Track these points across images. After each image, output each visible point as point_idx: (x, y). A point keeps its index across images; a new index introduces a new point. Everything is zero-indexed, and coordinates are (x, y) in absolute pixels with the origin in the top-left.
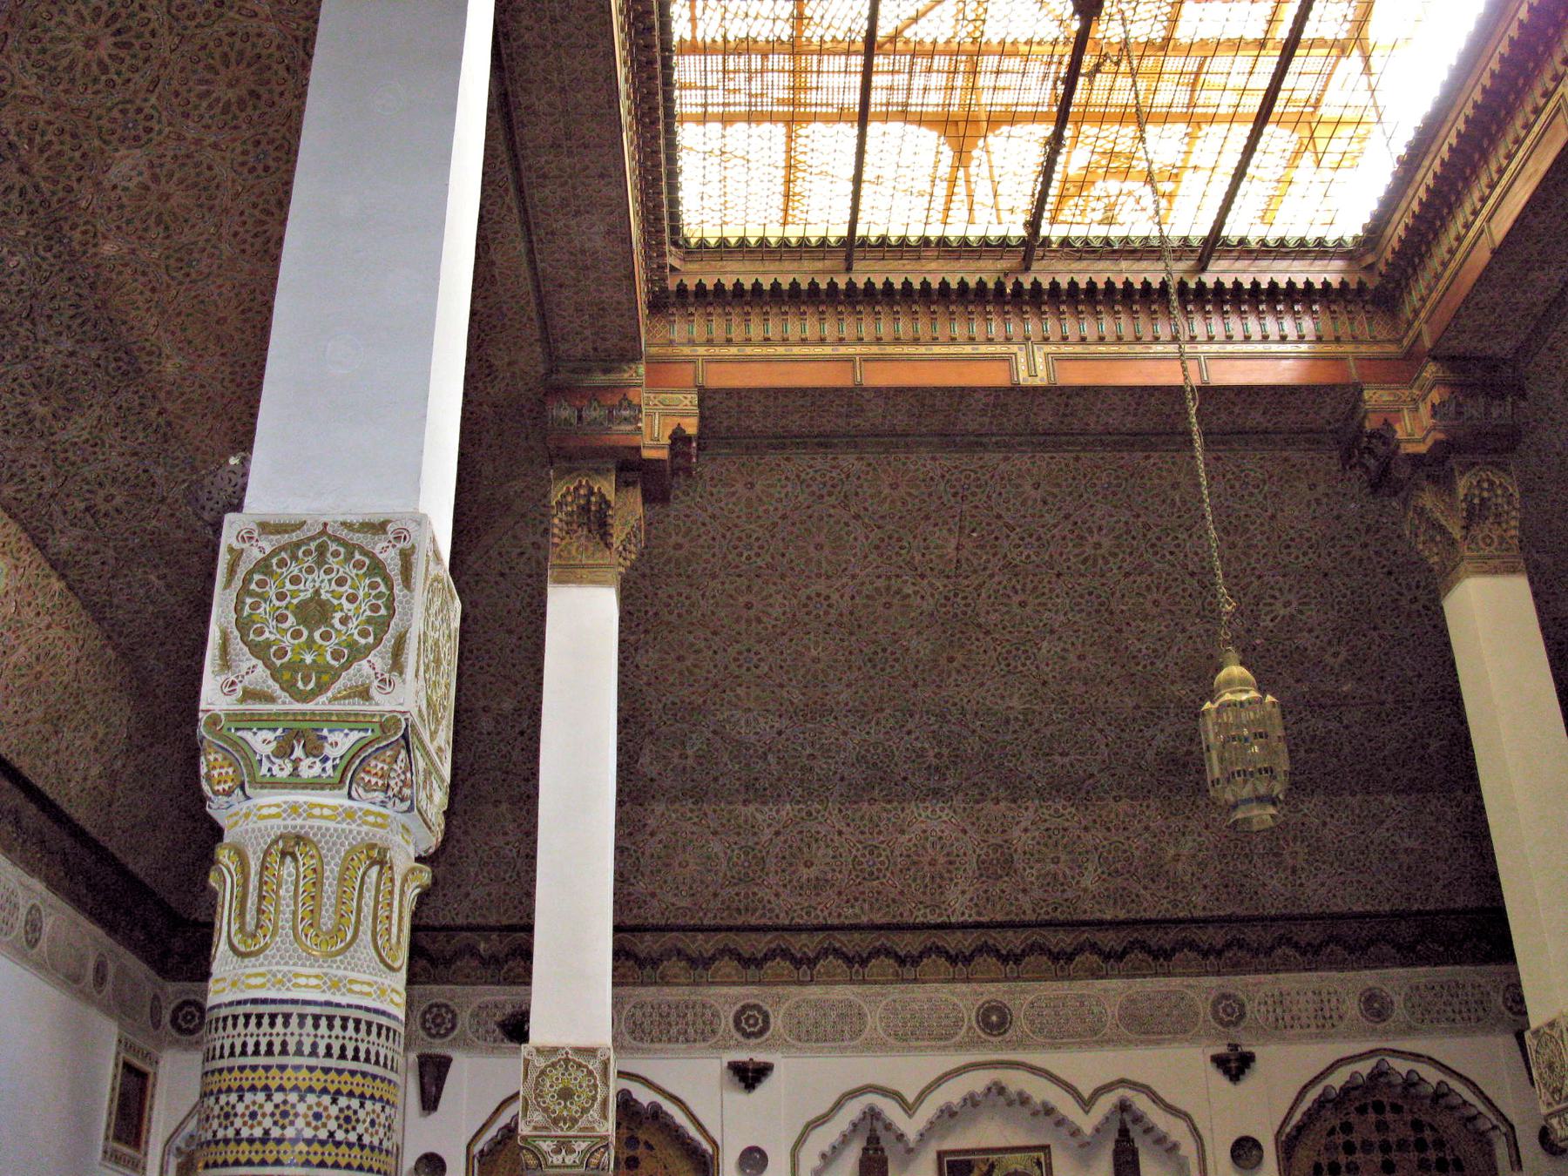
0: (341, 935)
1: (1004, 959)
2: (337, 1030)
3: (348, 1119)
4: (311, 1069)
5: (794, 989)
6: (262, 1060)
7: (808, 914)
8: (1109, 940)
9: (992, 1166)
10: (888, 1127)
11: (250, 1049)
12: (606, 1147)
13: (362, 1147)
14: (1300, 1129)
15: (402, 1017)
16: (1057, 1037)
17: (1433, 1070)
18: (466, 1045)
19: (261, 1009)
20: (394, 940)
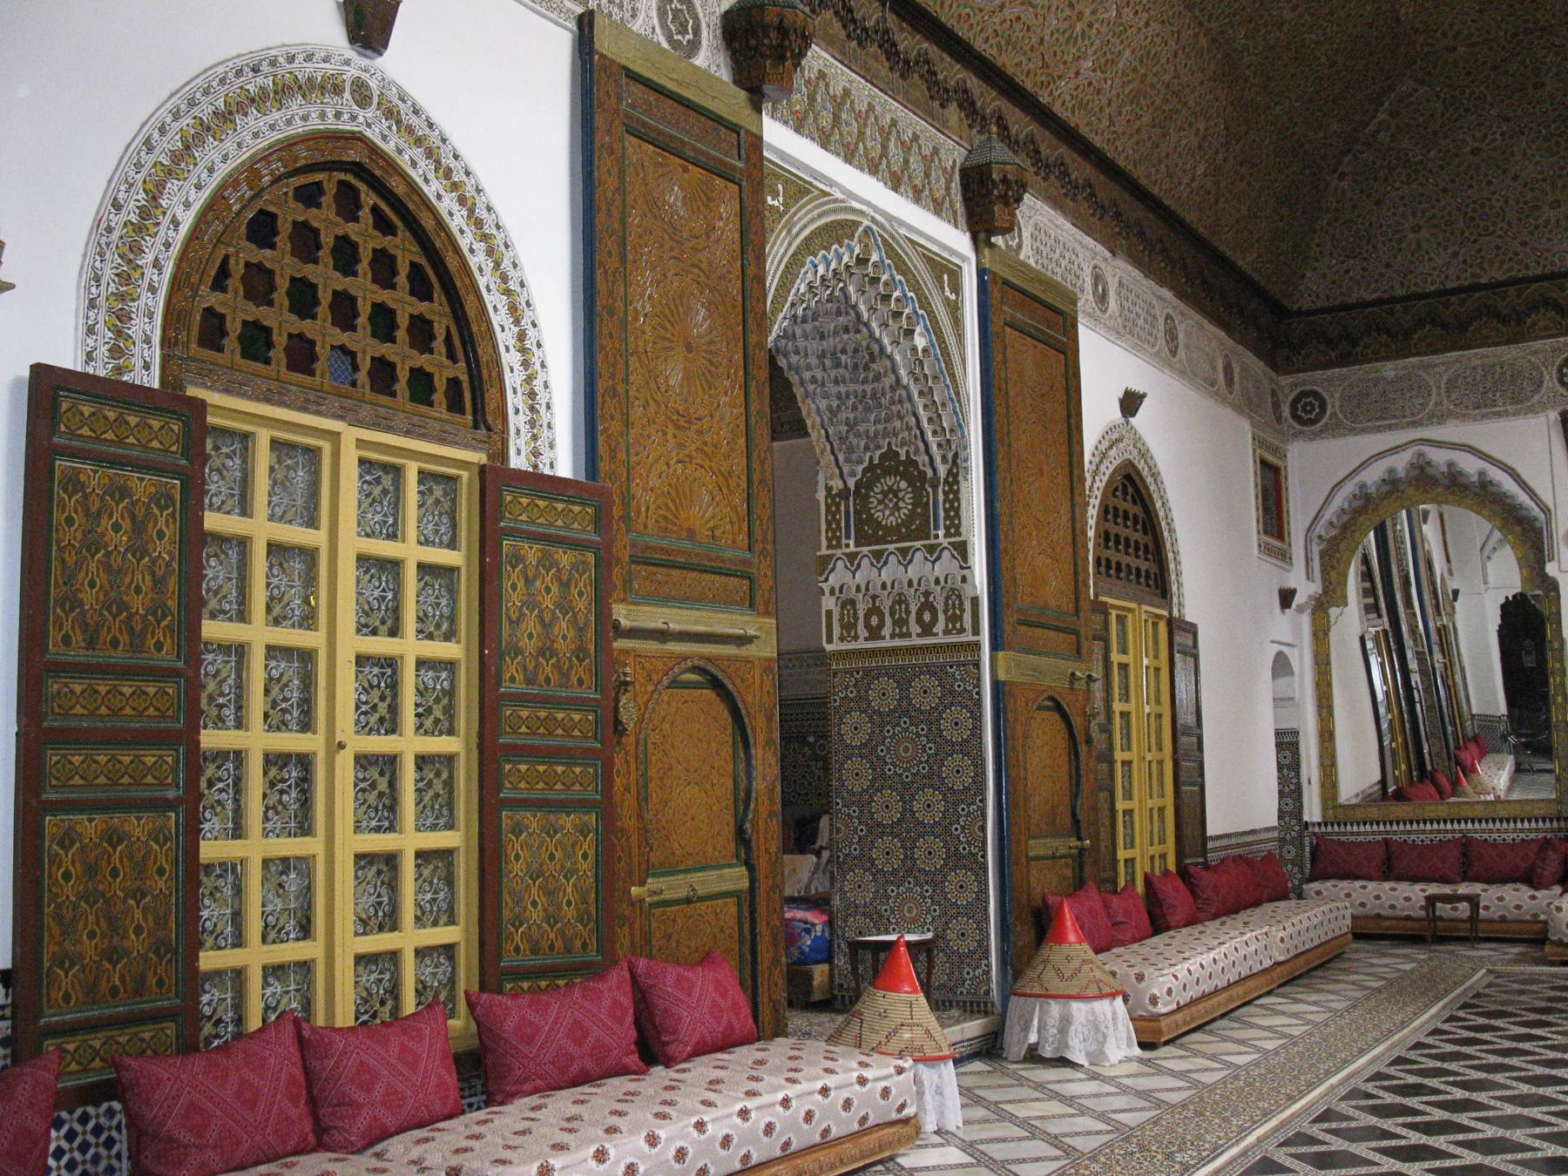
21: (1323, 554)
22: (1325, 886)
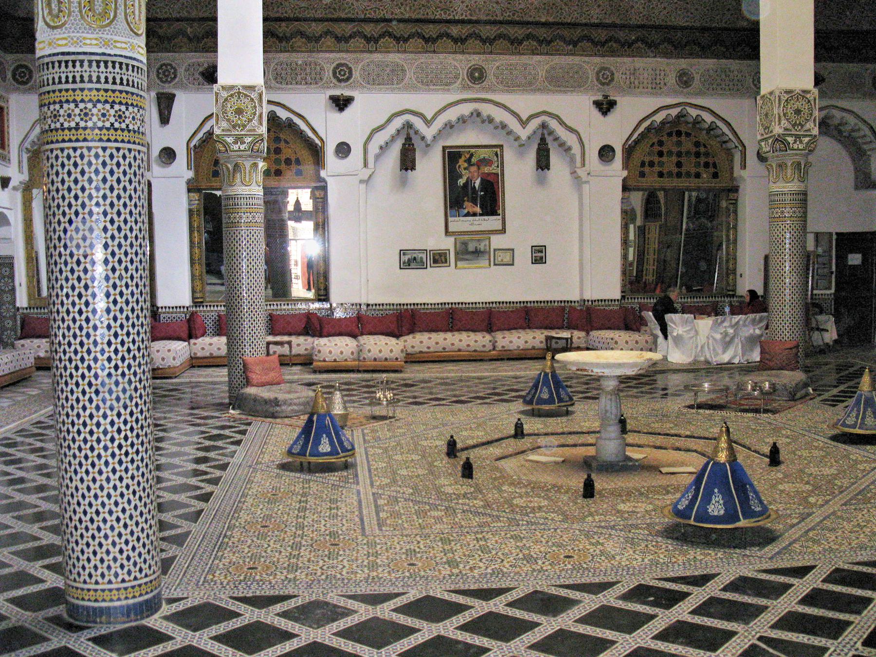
0: (107, 15)
1: (484, 41)
2: (110, 69)
3: (120, 116)
4: (98, 90)
5: (366, 55)
6: (70, 86)
7: (375, 12)
8: (542, 33)
9: (472, 155)
10: (416, 132)
11: (63, 80)
12: (262, 140)
13: (129, 131)
14: (636, 142)
15: (145, 61)
16: (511, 86)
17: (708, 114)
18: (183, 87)
19: (67, 58)
20: (137, 18)
21: (29, 159)
22: (27, 342)
